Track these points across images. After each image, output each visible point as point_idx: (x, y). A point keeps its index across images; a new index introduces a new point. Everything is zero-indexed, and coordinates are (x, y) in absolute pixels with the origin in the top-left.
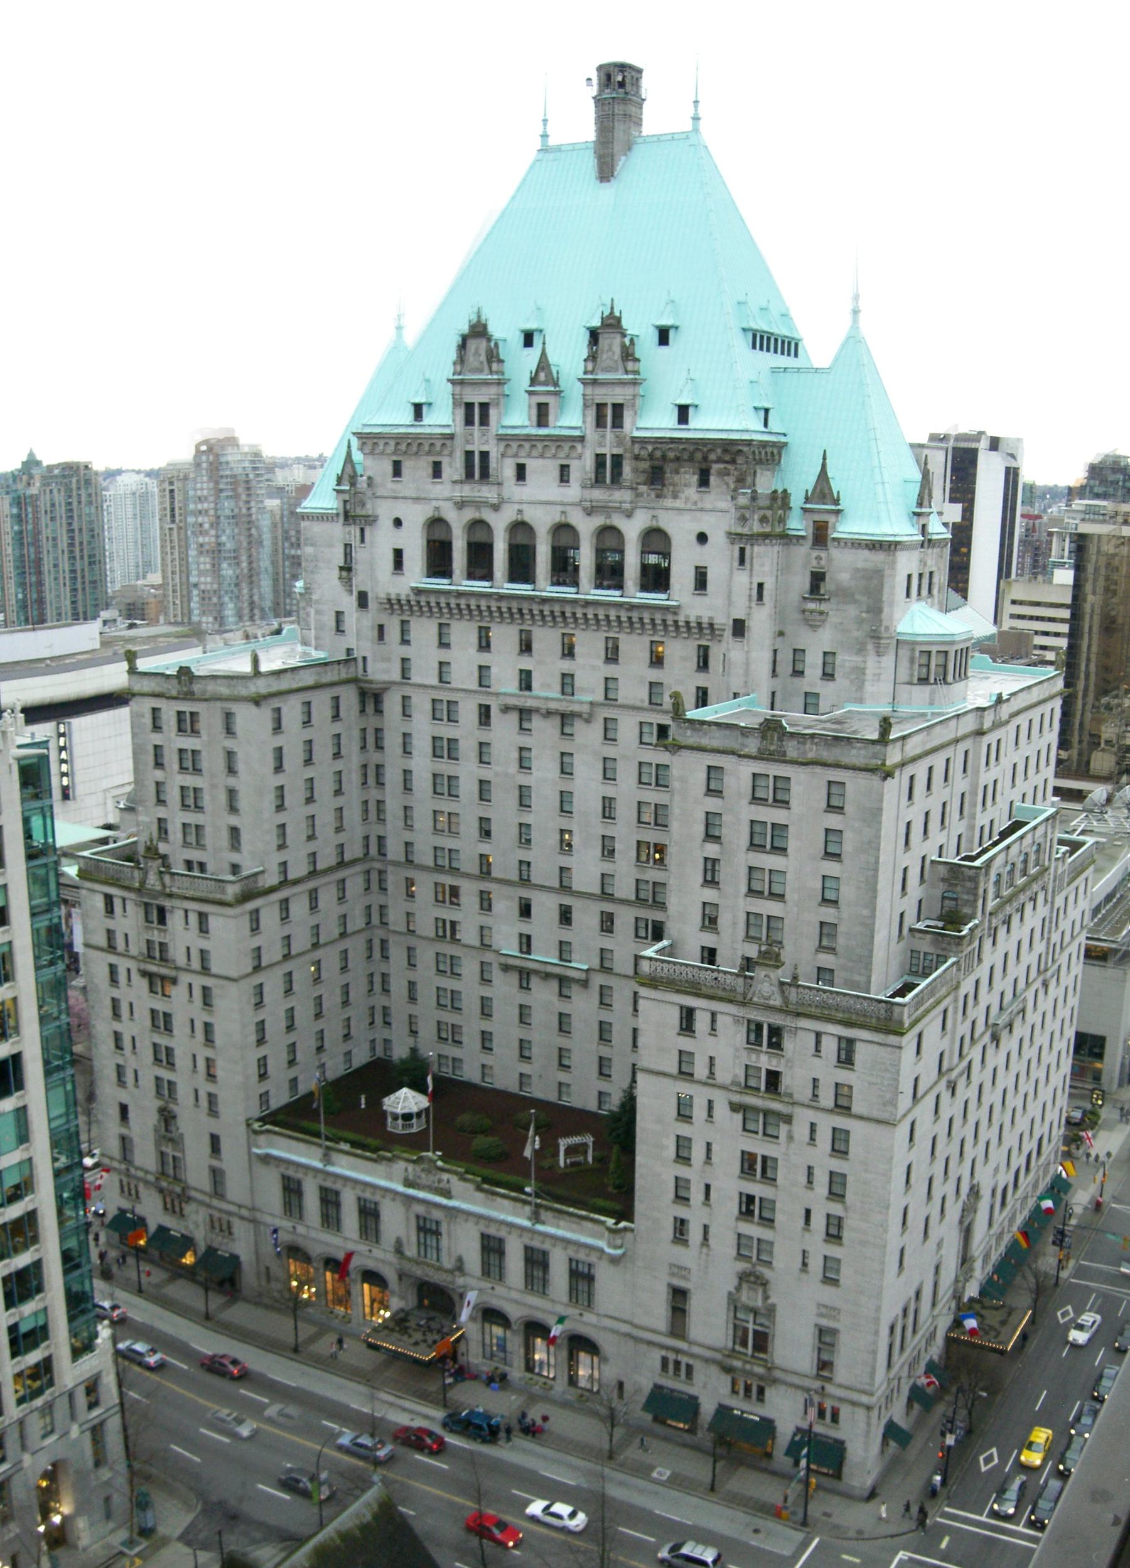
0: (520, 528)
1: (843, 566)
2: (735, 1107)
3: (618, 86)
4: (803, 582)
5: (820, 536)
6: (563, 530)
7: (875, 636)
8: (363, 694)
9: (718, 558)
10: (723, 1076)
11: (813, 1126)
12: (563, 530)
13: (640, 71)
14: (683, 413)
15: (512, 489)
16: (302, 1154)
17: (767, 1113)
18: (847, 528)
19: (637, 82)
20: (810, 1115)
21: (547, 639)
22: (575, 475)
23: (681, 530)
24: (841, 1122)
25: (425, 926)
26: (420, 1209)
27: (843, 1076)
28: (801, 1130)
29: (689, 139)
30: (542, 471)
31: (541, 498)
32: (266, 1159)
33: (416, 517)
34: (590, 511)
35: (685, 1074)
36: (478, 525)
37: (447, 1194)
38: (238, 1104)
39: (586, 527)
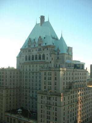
0: (33, 56)
1: (60, 56)
2: (46, 106)
3: (42, 18)
4: (57, 58)
5: (58, 54)
6: (36, 55)
7: (63, 62)
8: (20, 72)
9: (49, 56)
10: (45, 103)
11: (53, 108)
12: (36, 55)
13: (72, 48)
14: (46, 44)
15: (32, 52)
16: (9, 114)
17: (49, 106)
18: (60, 53)
19: (71, 51)
20: (53, 106)
21: (35, 65)
22: (37, 51)
23: (45, 54)
24: (56, 107)
25: (24, 94)
26: (19, 120)
27: (56, 102)
28: (52, 108)
29: (48, 22)
30: (34, 50)
31: (35, 53)
32: (6, 115)
33: (24, 56)
34: (38, 53)
35: (42, 103)
36: (30, 56)
37: (21, 118)
38: (4, 109)
39: (38, 55)
